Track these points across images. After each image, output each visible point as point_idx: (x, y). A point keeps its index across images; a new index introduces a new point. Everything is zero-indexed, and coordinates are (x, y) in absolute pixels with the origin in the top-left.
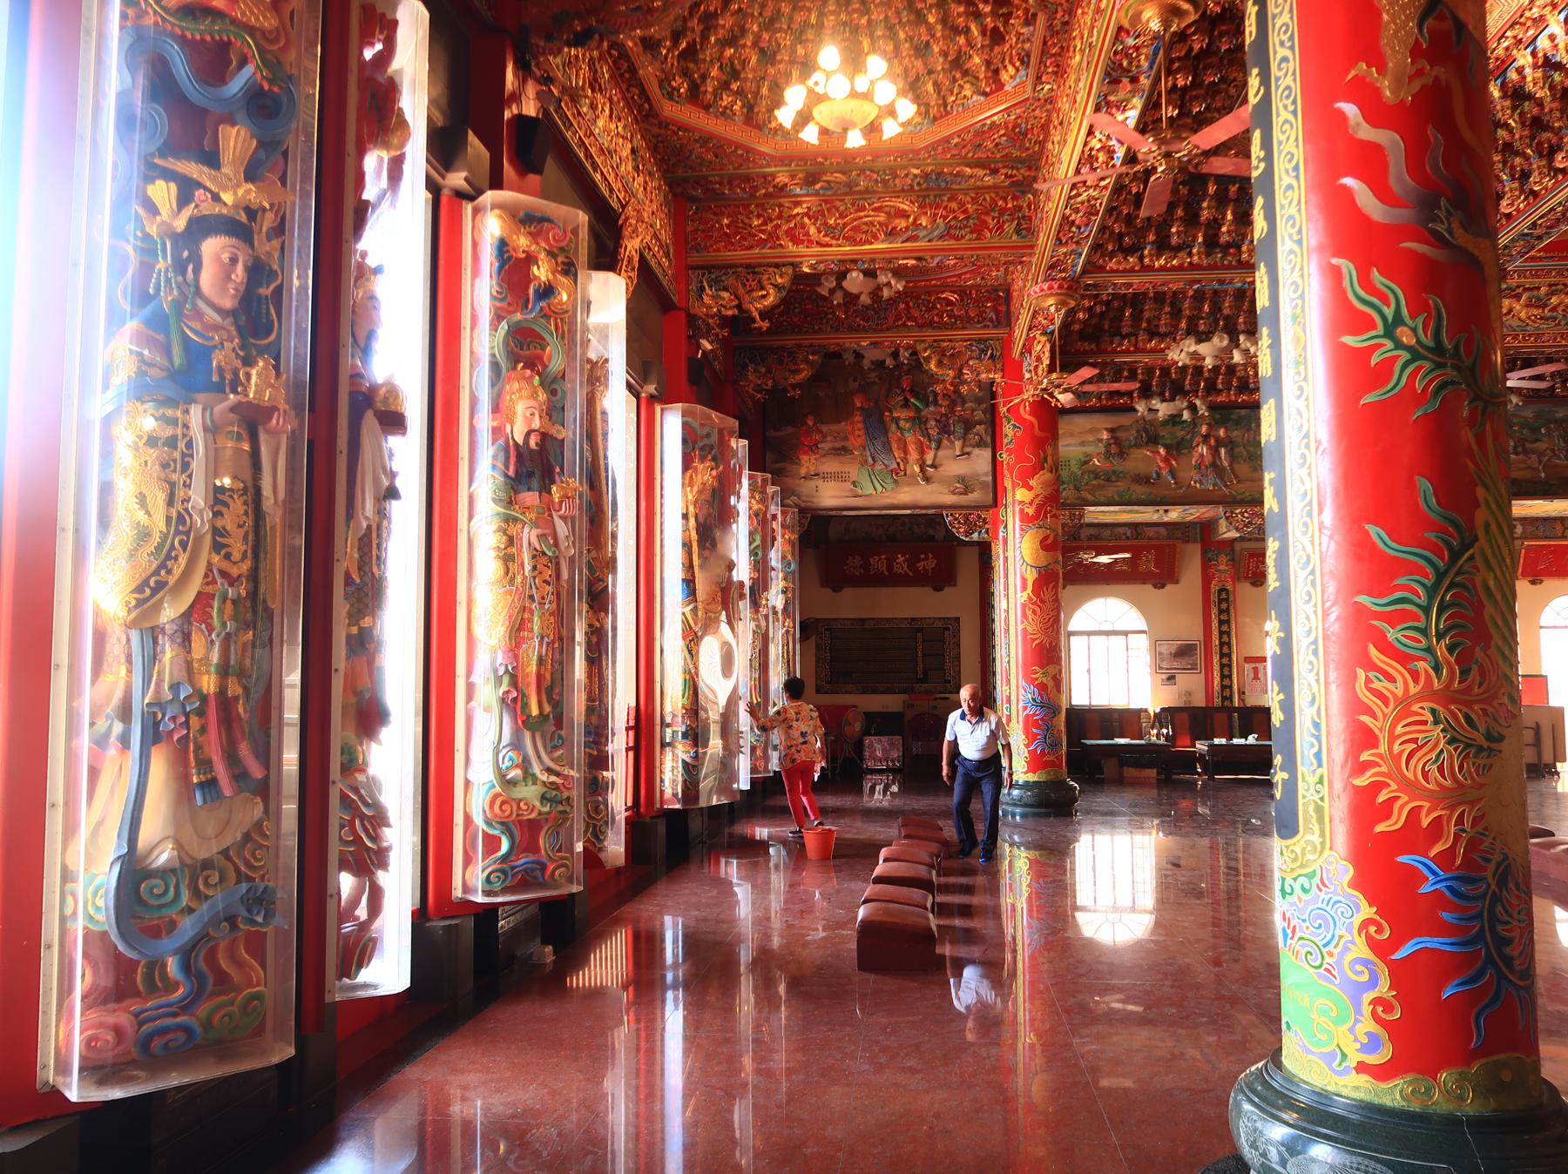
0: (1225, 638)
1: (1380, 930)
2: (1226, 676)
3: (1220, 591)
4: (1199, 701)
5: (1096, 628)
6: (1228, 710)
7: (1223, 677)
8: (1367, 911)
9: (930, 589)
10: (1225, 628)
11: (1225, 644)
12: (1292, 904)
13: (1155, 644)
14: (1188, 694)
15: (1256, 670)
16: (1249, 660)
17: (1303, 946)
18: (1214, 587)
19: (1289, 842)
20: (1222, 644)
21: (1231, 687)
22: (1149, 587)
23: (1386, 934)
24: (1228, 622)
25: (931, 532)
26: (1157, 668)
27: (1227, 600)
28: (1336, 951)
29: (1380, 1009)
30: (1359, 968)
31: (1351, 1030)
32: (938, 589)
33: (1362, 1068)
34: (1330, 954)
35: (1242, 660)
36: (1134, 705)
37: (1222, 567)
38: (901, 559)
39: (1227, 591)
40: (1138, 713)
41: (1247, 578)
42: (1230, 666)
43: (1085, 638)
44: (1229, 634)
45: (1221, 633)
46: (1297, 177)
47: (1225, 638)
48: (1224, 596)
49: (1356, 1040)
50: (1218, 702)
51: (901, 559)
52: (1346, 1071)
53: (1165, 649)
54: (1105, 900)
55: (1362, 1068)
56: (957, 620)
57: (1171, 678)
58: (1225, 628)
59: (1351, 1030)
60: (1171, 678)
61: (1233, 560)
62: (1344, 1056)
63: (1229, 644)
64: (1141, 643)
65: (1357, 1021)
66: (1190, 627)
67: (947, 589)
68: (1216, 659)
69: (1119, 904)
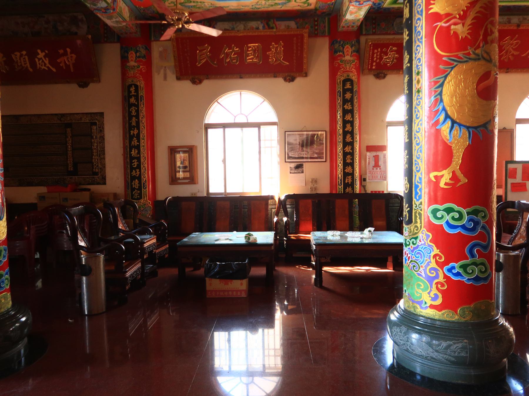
0: (348, 128)
1: (441, 258)
2: (348, 164)
3: (345, 82)
4: (324, 188)
5: (231, 120)
6: (349, 197)
7: (345, 164)
8: (436, 251)
9: (75, 86)
10: (348, 117)
11: (349, 135)
12: (409, 249)
13: (285, 134)
14: (315, 181)
15: (377, 158)
16: (370, 149)
17: (412, 264)
18: (340, 78)
19: (409, 226)
20: (345, 133)
21: (352, 174)
22: (280, 81)
23: (443, 260)
24: (351, 112)
25: (74, 29)
26: (287, 158)
27: (351, 90)
28: (424, 266)
29: (439, 286)
30: (432, 272)
31: (429, 293)
32: (84, 85)
33: (432, 307)
34: (422, 266)
35: (364, 149)
36: (265, 193)
37: (348, 58)
38: (41, 55)
39: (351, 81)
40: (265, 200)
41: (371, 70)
42: (352, 154)
43: (239, 130)
44: (352, 123)
45: (345, 123)
46: (415, 135)
47: (348, 128)
48: (348, 86)
49: (430, 296)
50: (340, 188)
51: (41, 55)
52: (426, 308)
53: (295, 139)
54: (239, 366)
55: (432, 307)
56: (102, 114)
57: (299, 167)
58: (348, 117)
59: (429, 293)
60: (299, 167)
61: (358, 51)
62: (426, 303)
63: (352, 133)
64: (272, 134)
65: (431, 290)
66: (317, 117)
67: (91, 85)
68: (340, 147)
69: (270, 348)
